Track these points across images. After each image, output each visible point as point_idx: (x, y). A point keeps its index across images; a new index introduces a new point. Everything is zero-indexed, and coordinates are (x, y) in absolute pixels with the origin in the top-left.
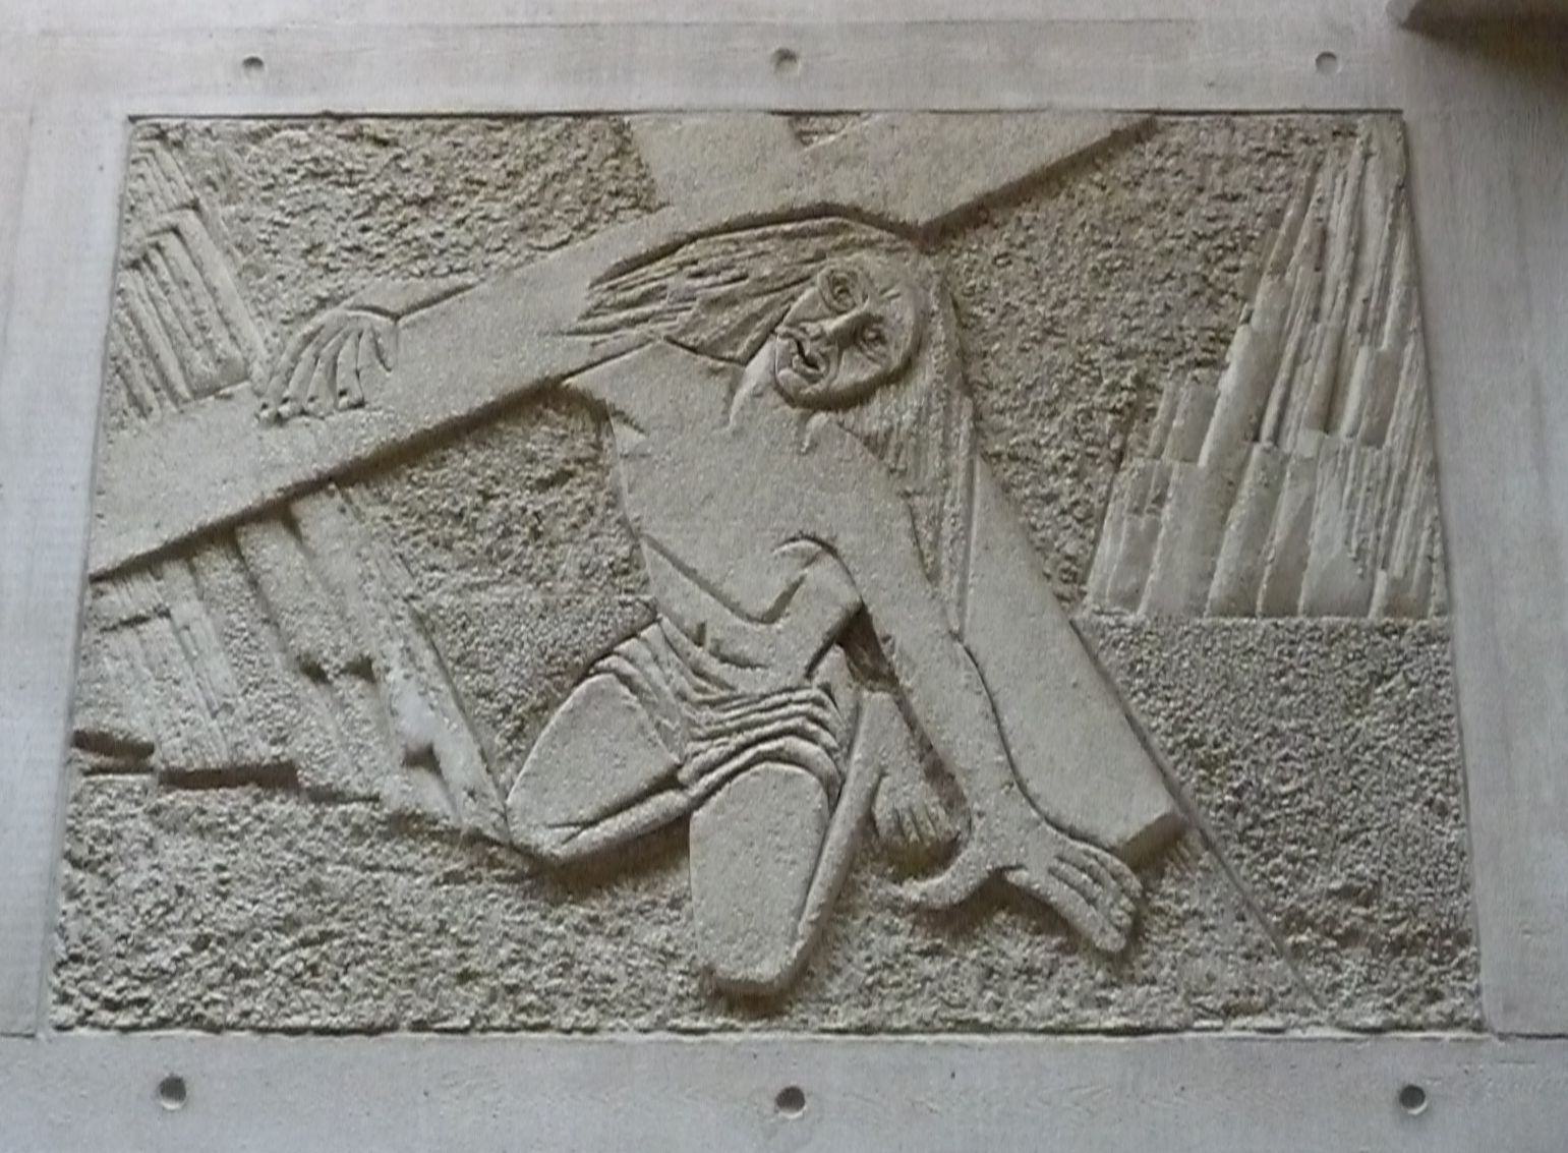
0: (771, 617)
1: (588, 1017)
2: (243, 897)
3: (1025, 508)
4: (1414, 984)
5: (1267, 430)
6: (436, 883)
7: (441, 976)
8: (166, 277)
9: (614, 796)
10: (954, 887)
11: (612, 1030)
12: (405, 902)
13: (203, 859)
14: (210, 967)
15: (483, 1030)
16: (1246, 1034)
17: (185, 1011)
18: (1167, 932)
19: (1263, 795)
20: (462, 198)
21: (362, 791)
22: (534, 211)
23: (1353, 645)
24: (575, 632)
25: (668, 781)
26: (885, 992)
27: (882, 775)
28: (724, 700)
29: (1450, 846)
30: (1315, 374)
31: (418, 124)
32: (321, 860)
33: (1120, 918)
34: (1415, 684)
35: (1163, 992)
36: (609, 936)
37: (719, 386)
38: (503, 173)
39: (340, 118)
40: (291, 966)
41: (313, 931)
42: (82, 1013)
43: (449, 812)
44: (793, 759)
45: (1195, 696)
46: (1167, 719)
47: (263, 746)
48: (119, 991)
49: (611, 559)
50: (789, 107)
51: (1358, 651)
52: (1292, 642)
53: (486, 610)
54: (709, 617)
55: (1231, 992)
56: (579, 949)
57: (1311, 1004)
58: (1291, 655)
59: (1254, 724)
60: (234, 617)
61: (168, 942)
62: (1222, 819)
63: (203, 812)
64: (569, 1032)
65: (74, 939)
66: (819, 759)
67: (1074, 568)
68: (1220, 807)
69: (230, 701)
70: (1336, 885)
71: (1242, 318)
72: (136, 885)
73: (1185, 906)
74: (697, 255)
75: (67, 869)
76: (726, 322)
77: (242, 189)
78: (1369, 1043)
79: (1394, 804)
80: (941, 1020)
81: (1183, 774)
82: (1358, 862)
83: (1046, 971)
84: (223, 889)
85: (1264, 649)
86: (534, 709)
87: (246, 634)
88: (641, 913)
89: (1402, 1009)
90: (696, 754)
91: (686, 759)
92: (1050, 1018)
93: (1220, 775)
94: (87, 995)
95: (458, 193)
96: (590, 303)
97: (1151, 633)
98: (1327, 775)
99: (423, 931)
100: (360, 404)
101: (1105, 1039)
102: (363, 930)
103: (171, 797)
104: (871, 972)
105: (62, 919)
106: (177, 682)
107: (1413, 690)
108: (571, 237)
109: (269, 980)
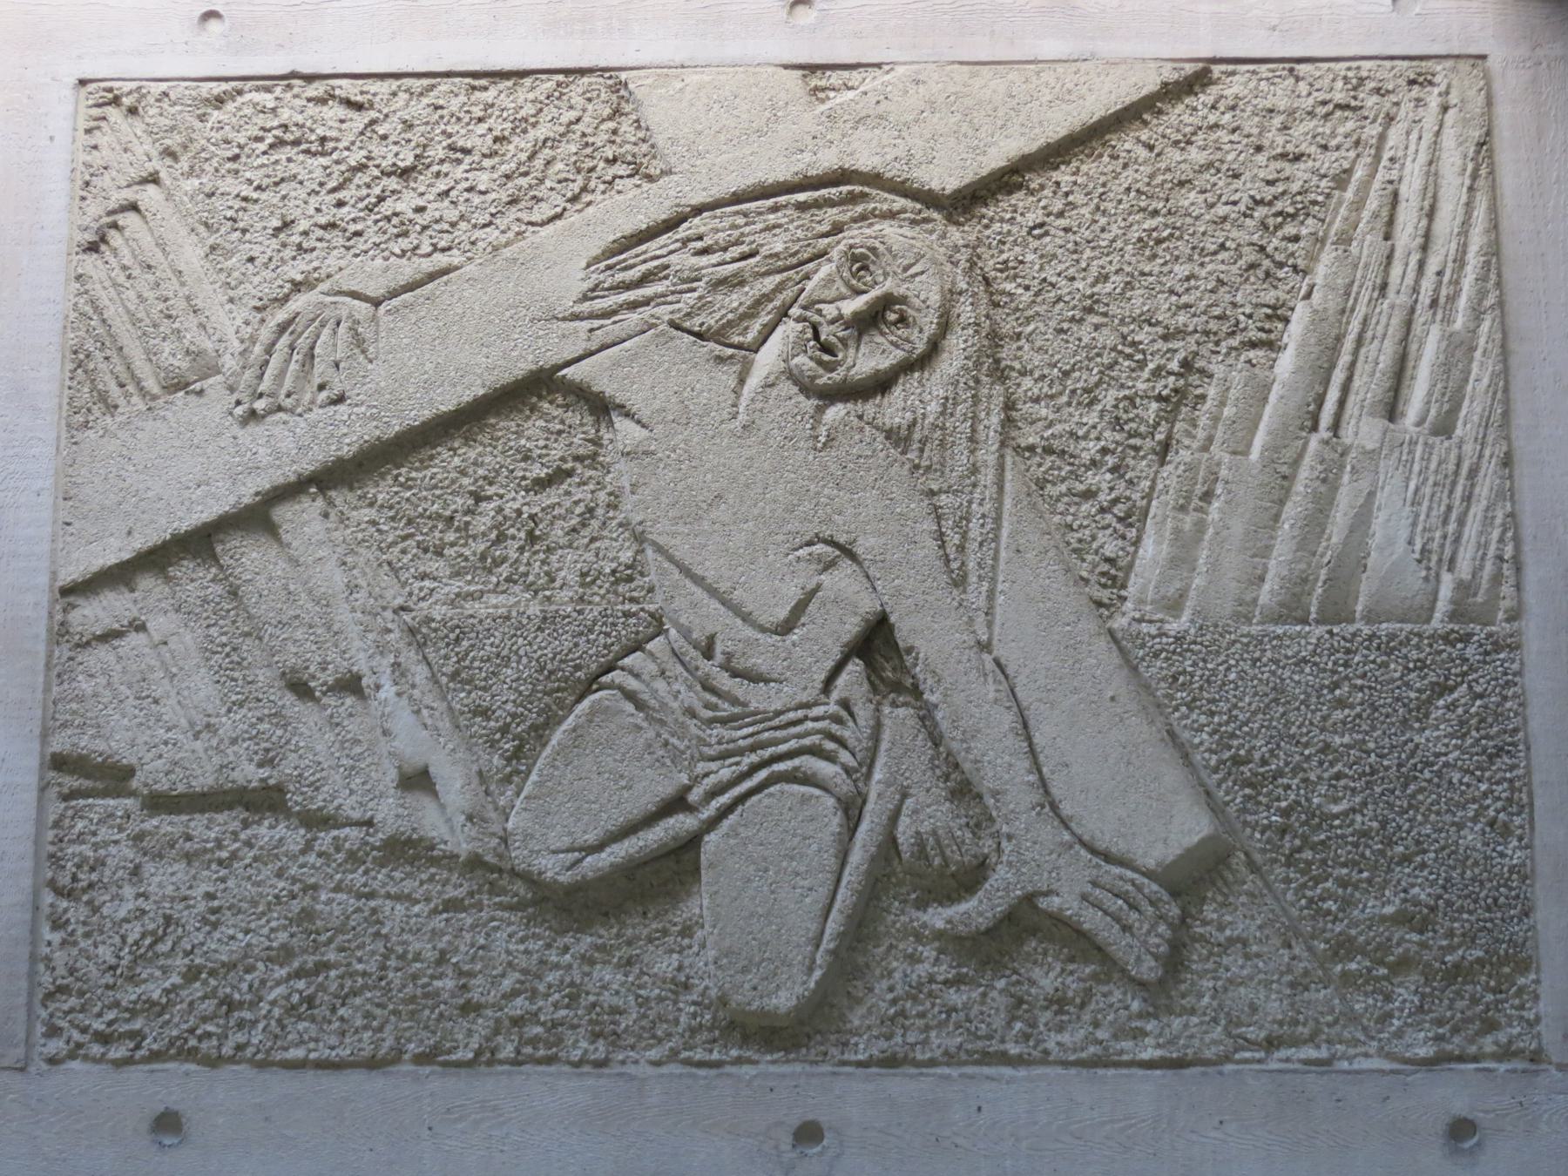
0: (786, 628)
2: (234, 926)
3: (1061, 507)
4: (1469, 1013)
5: (1326, 418)
6: (435, 911)
9: (615, 818)
10: (980, 914)
11: (623, 1062)
13: (191, 887)
15: (490, 1063)
18: (1208, 959)
19: (1314, 815)
20: (445, 168)
21: (356, 815)
22: (523, 182)
23: (1414, 655)
24: (576, 645)
25: (677, 803)
26: (907, 1023)
31: (394, 84)
32: (315, 887)
33: (1158, 946)
34: (1481, 696)
37: (727, 375)
39: (310, 78)
46: (1211, 734)
48: (110, 1023)
49: (614, 565)
51: (1419, 660)
52: (1348, 652)
53: (481, 622)
54: (719, 628)
59: (1304, 740)
60: (214, 631)
61: (158, 973)
63: (189, 838)
64: (577, 1065)
65: (61, 971)
67: (1113, 572)
68: (1269, 827)
69: (213, 720)
70: (1389, 910)
71: (1303, 292)
72: (122, 913)
73: (1228, 932)
74: (702, 229)
75: (48, 897)
77: (207, 160)
79: (1453, 824)
80: (967, 1051)
81: (1227, 793)
82: (1413, 886)
83: (1078, 1000)
85: (1317, 659)
86: (534, 728)
87: (228, 649)
89: (1456, 1040)
90: (707, 775)
91: (696, 780)
94: (77, 1027)
95: (442, 161)
97: (1195, 643)
100: (340, 399)
101: (1141, 1072)
103: (155, 822)
104: (894, 1002)
105: (48, 950)
106: (156, 702)
107: (1478, 703)
108: (565, 209)
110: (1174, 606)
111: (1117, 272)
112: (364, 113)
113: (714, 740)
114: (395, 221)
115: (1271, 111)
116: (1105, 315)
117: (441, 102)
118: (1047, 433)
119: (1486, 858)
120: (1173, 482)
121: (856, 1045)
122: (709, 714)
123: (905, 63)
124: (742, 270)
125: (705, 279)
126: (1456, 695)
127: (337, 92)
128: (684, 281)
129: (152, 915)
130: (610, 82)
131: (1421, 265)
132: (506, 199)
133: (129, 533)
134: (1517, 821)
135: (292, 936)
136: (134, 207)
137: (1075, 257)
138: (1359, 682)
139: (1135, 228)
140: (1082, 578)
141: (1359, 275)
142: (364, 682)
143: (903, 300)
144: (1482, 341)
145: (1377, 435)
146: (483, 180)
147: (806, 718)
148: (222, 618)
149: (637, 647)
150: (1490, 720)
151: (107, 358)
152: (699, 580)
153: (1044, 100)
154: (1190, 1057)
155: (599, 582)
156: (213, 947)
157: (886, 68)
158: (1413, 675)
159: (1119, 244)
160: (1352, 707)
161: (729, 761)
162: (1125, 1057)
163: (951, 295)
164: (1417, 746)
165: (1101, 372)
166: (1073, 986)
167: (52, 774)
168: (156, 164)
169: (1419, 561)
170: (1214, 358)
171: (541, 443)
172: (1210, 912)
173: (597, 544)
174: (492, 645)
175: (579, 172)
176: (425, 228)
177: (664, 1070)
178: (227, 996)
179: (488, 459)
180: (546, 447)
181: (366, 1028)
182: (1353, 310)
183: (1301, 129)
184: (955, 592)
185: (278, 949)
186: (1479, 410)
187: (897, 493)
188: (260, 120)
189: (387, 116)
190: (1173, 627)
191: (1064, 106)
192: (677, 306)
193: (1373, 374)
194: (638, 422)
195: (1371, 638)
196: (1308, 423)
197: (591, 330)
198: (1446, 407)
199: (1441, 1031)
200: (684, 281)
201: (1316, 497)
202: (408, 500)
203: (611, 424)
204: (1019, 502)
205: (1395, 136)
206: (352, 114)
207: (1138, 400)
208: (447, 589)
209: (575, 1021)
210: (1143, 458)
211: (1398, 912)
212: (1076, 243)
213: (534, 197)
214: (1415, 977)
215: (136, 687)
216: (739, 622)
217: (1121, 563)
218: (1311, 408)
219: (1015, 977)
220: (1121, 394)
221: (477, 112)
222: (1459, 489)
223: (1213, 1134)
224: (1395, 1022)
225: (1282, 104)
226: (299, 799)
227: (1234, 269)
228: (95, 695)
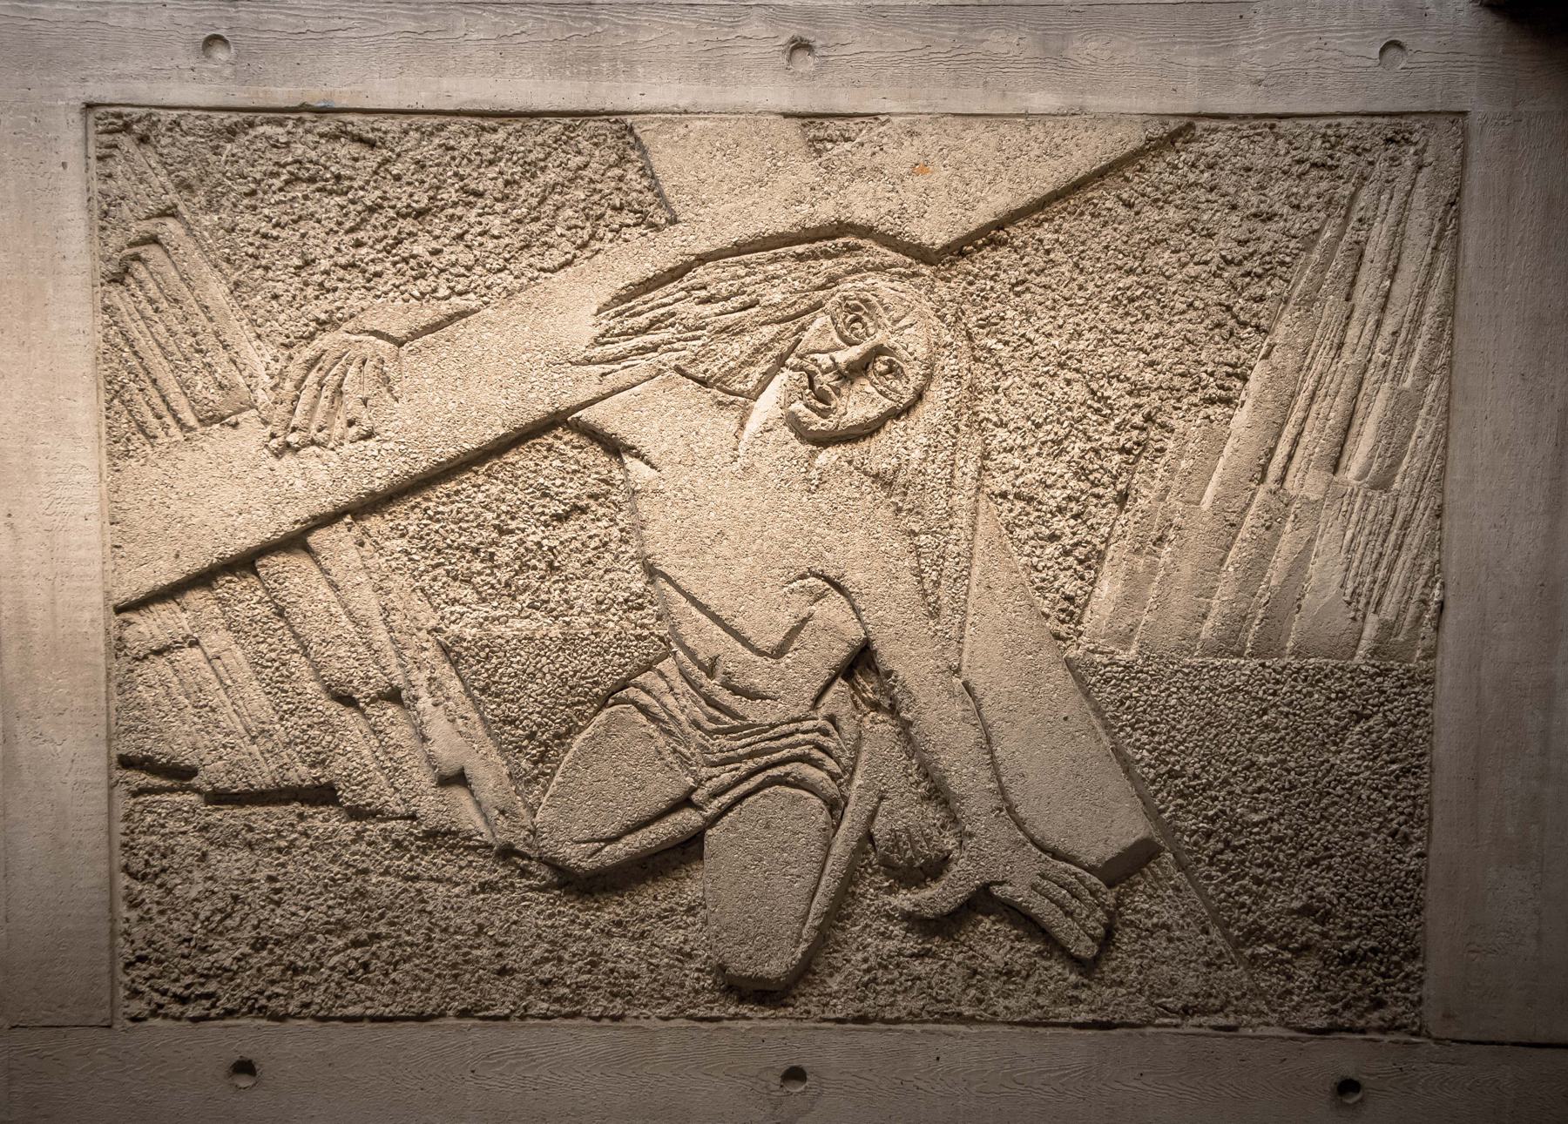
0: (779, 652)
1: (615, 1007)
2: (296, 905)
3: (1027, 549)
4: (1360, 993)
5: (1274, 470)
6: (474, 892)
7: (481, 972)
8: (153, 291)
9: (634, 814)
10: (944, 899)
11: (637, 1017)
12: (445, 908)
13: (254, 871)
14: (270, 965)
15: (522, 1018)
16: (1202, 1030)
17: (250, 1003)
18: (1136, 942)
19: (1236, 823)
20: (459, 211)
21: (401, 810)
22: (535, 227)
23: (1337, 686)
24: (594, 664)
25: (685, 802)
26: (878, 988)
27: (881, 799)
28: (733, 730)
29: (1408, 874)
30: (1331, 410)
31: (405, 122)
32: (366, 871)
33: (1095, 929)
34: (1394, 724)
35: (1129, 993)
36: (633, 939)
37: (729, 421)
38: (500, 182)
39: (322, 111)
40: (345, 964)
41: (363, 933)
42: (153, 1006)
43: (483, 829)
44: (799, 784)
45: (1179, 730)
46: (1150, 752)
47: (303, 769)
48: (188, 987)
49: (627, 595)
50: (800, 109)
51: (1341, 691)
52: (1277, 682)
53: (508, 642)
54: (721, 651)
55: (1190, 994)
56: (605, 949)
57: (1265, 1008)
58: (1275, 694)
59: (1232, 758)
60: (263, 647)
61: (228, 944)
62: (1196, 844)
63: (251, 829)
64: (598, 1019)
65: (140, 943)
66: (824, 784)
67: (1072, 608)
68: (1195, 832)
69: (267, 727)
70: (1296, 904)
71: (1263, 352)
72: (193, 894)
73: (1155, 920)
74: (707, 279)
75: (124, 880)
76: (737, 353)
77: (223, 194)
78: (1315, 1043)
79: (1360, 834)
80: (929, 1012)
81: (1162, 802)
82: (1319, 885)
83: (1024, 973)
84: (276, 898)
85: (1249, 688)
86: (557, 736)
87: (277, 664)
88: (661, 918)
89: (1347, 1014)
90: (710, 778)
91: (700, 783)
92: (1026, 1013)
93: (1197, 804)
94: (157, 991)
95: (455, 204)
96: (598, 331)
97: (1141, 671)
98: (1299, 806)
99: (463, 934)
100: (369, 435)
101: (1075, 1032)
102: (408, 933)
103: (218, 815)
104: (868, 971)
105: (126, 925)
106: (213, 710)
107: (1391, 730)
108: (575, 256)
109: (324, 976)
110: (1125, 640)
111: (1090, 329)
112: (377, 152)
113: (715, 749)
114: (413, 262)
115: (1248, 170)
116: (1077, 371)
117: (452, 143)
118: (1018, 482)
119: (1386, 863)
120: (1130, 529)
121: (835, 1005)
122: (712, 726)
123: (900, 114)
124: (741, 320)
125: (710, 328)
126: (1371, 723)
127: (349, 128)
128: (689, 329)
129: (220, 895)
130: (616, 127)
131: (1379, 324)
132: (518, 245)
133: (177, 556)
134: (1417, 832)
135: (348, 912)
136: (154, 240)
137: (1053, 313)
138: (1286, 709)
139: (1111, 286)
140: (1043, 613)
141: (1318, 336)
142: (404, 694)
143: (890, 351)
144: (1429, 399)
145: (1322, 487)
146: (496, 224)
147: (797, 731)
148: (271, 636)
149: (649, 667)
150: (1400, 745)
151: (141, 390)
152: (703, 608)
153: (1032, 154)
154: (1116, 1022)
155: (613, 610)
156: (277, 921)
157: (883, 118)
158: (1334, 704)
159: (1095, 302)
160: (1277, 730)
161: (728, 767)
162: (1062, 1020)
163: (937, 347)
164: (1333, 766)
165: (1072, 425)
166: (1020, 961)
167: (118, 774)
168: (172, 197)
169: (1349, 603)
170: (1175, 414)
171: (558, 482)
172: (1140, 901)
173: (611, 575)
174: (518, 662)
175: (587, 219)
176: (442, 271)
177: (672, 1023)
178: (292, 963)
179: (509, 496)
180: (563, 485)
181: (414, 988)
182: (1309, 368)
183: (1274, 191)
184: (931, 622)
185: (335, 924)
186: (1418, 465)
187: (882, 533)
188: (273, 155)
189: (399, 155)
190: (1123, 657)
191: (1051, 162)
192: (683, 353)
193: (1321, 431)
194: (648, 463)
195: (1298, 671)
196: (1258, 476)
197: (604, 375)
198: (1388, 462)
199: (1334, 1007)
200: (689, 329)
201: (1259, 542)
202: (437, 532)
203: (622, 464)
204: (992, 543)
205: (1364, 197)
206: (365, 151)
207: (1103, 452)
208: (475, 614)
209: (596, 984)
210: (1104, 506)
211: (1304, 907)
212: (1054, 301)
213: (545, 243)
214: (1314, 962)
215: (193, 697)
216: (739, 645)
217: (1078, 601)
218: (1261, 462)
219: (971, 953)
220: (1088, 446)
221: (487, 154)
222: (1392, 537)
223: (1134, 1084)
224: (1295, 998)
225: (1260, 163)
226: (350, 795)
227: (1201, 329)
228: (156, 704)
